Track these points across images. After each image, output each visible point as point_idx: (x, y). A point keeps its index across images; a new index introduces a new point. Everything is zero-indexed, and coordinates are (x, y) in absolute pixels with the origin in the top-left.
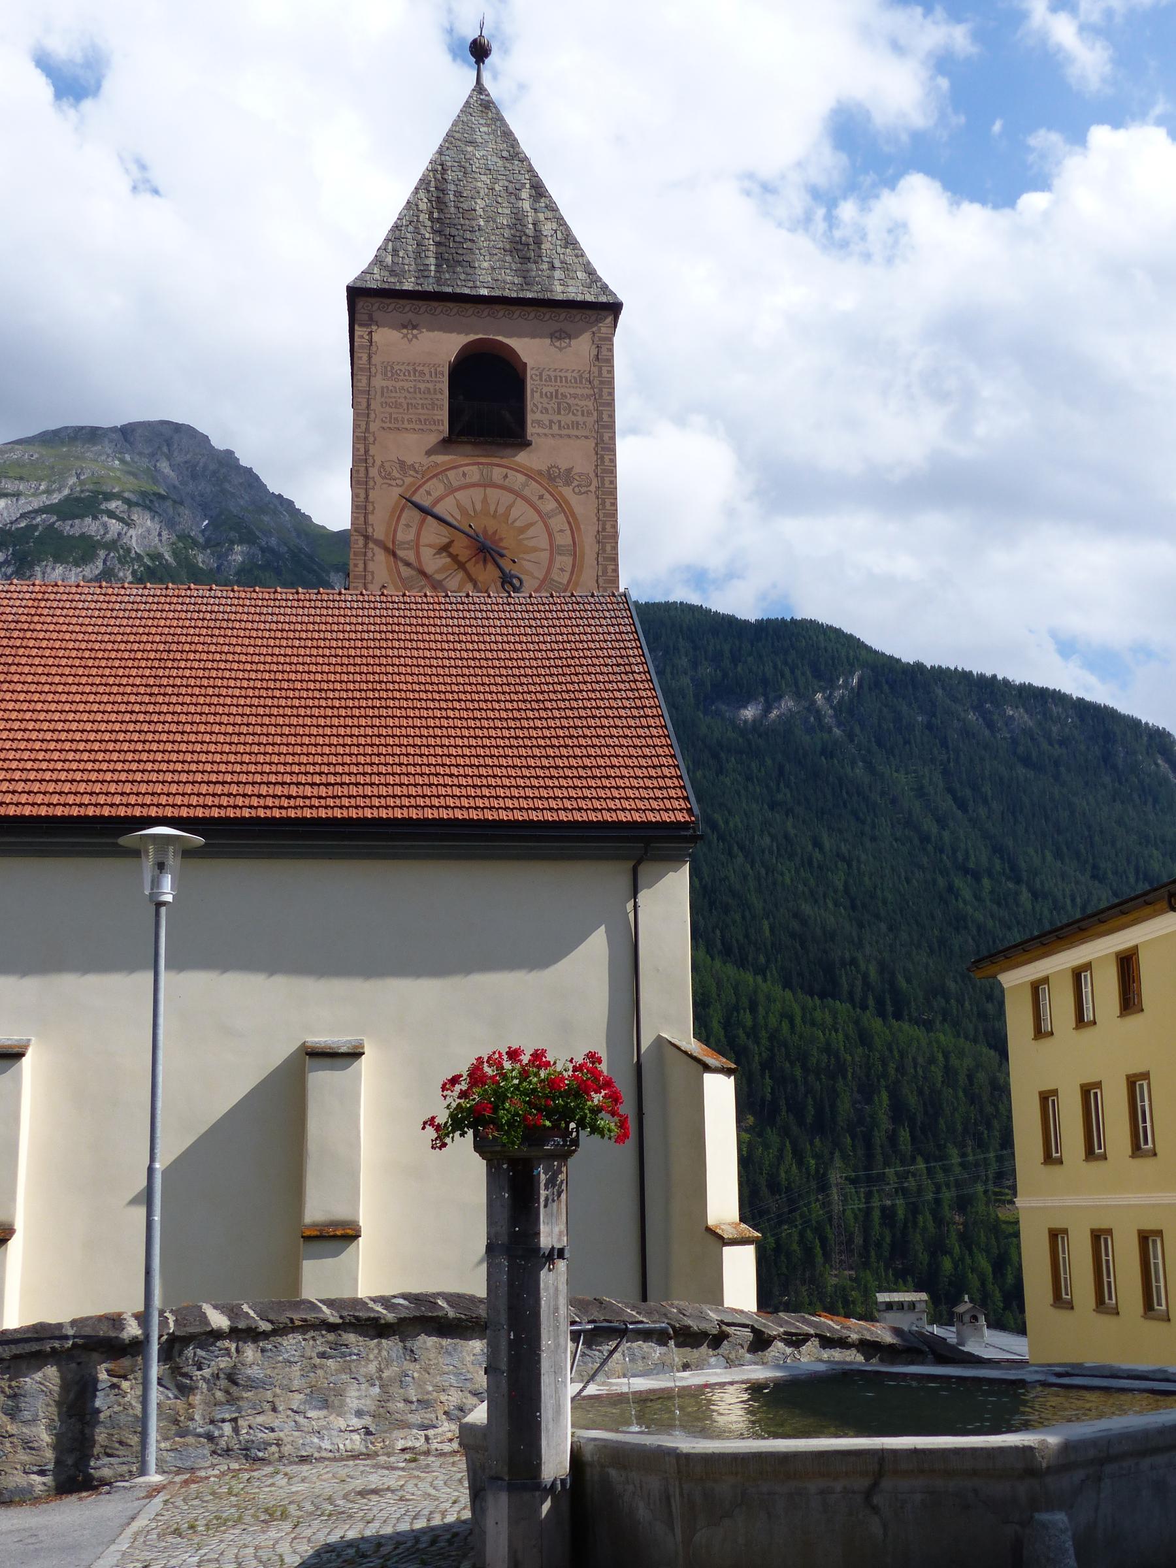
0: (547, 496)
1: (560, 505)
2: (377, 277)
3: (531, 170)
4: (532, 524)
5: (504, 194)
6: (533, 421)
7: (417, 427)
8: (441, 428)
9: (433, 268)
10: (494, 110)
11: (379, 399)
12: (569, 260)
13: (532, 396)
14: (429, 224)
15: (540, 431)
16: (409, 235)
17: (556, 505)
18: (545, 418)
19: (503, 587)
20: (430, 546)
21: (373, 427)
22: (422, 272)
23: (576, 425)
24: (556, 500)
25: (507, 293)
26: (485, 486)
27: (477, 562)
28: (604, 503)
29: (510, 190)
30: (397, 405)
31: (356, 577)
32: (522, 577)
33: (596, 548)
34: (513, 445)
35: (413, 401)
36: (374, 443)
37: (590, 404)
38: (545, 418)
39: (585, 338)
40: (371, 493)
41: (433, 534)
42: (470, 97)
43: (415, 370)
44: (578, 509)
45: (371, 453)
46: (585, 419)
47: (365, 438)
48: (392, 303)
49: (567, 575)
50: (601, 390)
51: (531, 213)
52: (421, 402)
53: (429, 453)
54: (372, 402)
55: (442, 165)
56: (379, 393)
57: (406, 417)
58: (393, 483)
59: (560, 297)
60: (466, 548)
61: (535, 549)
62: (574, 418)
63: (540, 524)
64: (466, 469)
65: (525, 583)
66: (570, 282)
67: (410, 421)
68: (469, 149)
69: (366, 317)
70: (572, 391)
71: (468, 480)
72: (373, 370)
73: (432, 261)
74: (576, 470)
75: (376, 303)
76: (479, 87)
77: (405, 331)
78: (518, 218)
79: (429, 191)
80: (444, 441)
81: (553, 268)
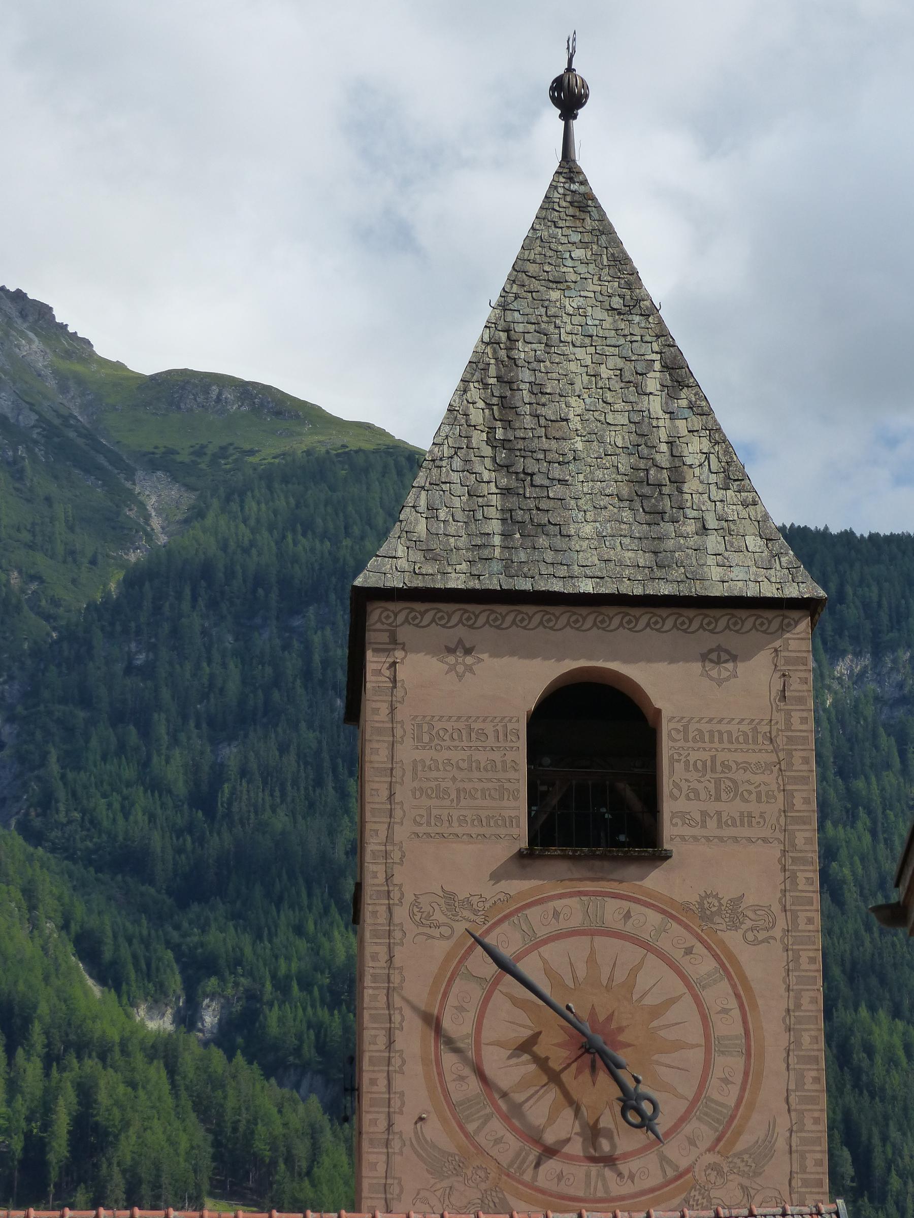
0: (699, 948)
1: (722, 965)
2: (402, 564)
3: (662, 333)
5: (616, 385)
7: (474, 831)
8: (515, 831)
9: (497, 540)
10: (595, 215)
12: (731, 512)
14: (487, 451)
15: (687, 831)
16: (455, 477)
17: (714, 964)
18: (694, 808)
19: (624, 1115)
20: (499, 1044)
22: (479, 549)
23: (747, 819)
24: (716, 957)
25: (626, 588)
26: (592, 933)
27: (579, 1071)
28: (797, 959)
29: (628, 376)
32: (655, 1095)
34: (639, 859)
35: (468, 786)
36: (401, 863)
38: (694, 808)
39: (763, 658)
40: (398, 951)
41: (508, 1019)
42: (553, 187)
45: (397, 880)
48: (429, 611)
49: (735, 1091)
50: (790, 753)
51: (664, 421)
53: (496, 877)
54: (398, 789)
55: (507, 331)
56: (409, 774)
58: (436, 932)
59: (717, 591)
60: (558, 1045)
61: (679, 1046)
62: (744, 807)
64: (558, 904)
65: (661, 1106)
66: (735, 558)
67: (462, 821)
68: (555, 295)
69: (385, 637)
70: (740, 757)
72: (399, 732)
73: (495, 526)
74: (750, 900)
75: (401, 610)
76: (569, 169)
77: (451, 659)
78: (642, 429)
79: (486, 386)
81: (704, 529)
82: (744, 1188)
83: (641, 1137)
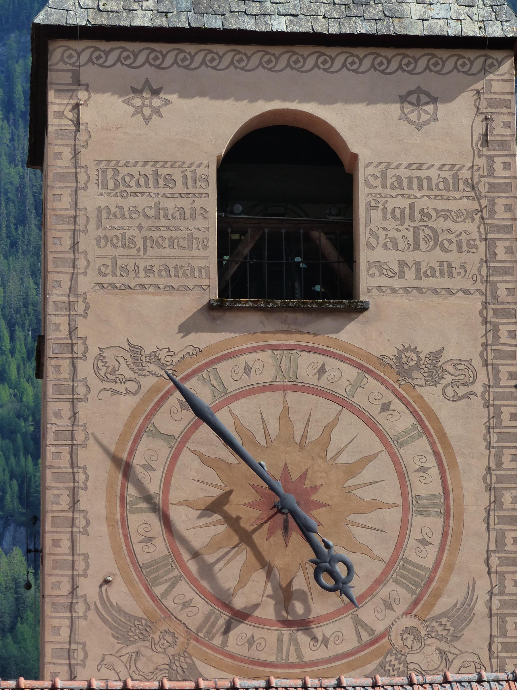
0: (397, 405)
4: (368, 459)
6: (370, 265)
7: (161, 282)
8: (205, 282)
11: (93, 232)
13: (369, 219)
15: (384, 282)
18: (392, 258)
20: (188, 504)
21: (84, 284)
23: (447, 269)
24: (414, 413)
26: (285, 389)
27: (271, 532)
28: (498, 415)
30: (127, 242)
31: (57, 565)
33: (485, 499)
35: (155, 234)
36: (85, 315)
37: (472, 228)
38: (392, 258)
39: (465, 101)
40: (81, 407)
43: (157, 175)
44: (453, 428)
45: (80, 333)
46: (464, 257)
47: (70, 306)
49: (432, 552)
50: (492, 201)
52: (167, 234)
53: (185, 329)
56: (93, 223)
57: (142, 264)
59: (417, 30)
60: (250, 505)
61: (375, 505)
62: (445, 257)
63: (385, 457)
64: (250, 358)
65: (356, 569)
67: (149, 271)
69: (67, 78)
70: (440, 204)
71: (255, 380)
72: (82, 178)
74: (449, 354)
77: (137, 102)
80: (210, 307)
82: (442, 653)
83: (335, 600)
